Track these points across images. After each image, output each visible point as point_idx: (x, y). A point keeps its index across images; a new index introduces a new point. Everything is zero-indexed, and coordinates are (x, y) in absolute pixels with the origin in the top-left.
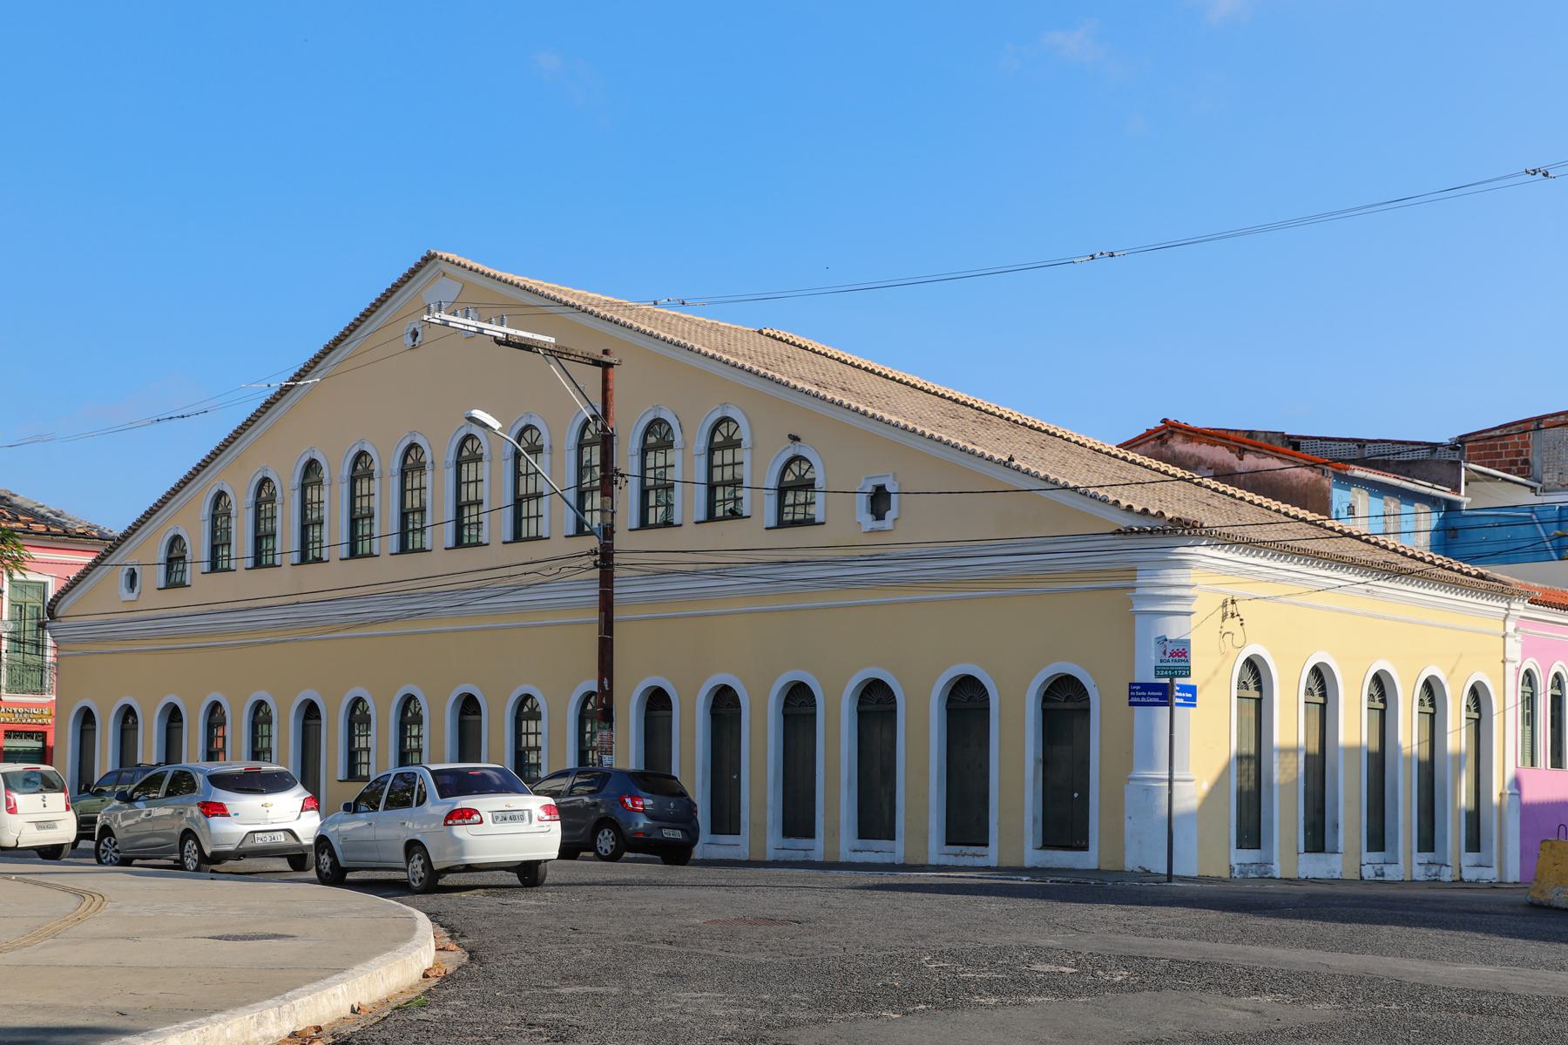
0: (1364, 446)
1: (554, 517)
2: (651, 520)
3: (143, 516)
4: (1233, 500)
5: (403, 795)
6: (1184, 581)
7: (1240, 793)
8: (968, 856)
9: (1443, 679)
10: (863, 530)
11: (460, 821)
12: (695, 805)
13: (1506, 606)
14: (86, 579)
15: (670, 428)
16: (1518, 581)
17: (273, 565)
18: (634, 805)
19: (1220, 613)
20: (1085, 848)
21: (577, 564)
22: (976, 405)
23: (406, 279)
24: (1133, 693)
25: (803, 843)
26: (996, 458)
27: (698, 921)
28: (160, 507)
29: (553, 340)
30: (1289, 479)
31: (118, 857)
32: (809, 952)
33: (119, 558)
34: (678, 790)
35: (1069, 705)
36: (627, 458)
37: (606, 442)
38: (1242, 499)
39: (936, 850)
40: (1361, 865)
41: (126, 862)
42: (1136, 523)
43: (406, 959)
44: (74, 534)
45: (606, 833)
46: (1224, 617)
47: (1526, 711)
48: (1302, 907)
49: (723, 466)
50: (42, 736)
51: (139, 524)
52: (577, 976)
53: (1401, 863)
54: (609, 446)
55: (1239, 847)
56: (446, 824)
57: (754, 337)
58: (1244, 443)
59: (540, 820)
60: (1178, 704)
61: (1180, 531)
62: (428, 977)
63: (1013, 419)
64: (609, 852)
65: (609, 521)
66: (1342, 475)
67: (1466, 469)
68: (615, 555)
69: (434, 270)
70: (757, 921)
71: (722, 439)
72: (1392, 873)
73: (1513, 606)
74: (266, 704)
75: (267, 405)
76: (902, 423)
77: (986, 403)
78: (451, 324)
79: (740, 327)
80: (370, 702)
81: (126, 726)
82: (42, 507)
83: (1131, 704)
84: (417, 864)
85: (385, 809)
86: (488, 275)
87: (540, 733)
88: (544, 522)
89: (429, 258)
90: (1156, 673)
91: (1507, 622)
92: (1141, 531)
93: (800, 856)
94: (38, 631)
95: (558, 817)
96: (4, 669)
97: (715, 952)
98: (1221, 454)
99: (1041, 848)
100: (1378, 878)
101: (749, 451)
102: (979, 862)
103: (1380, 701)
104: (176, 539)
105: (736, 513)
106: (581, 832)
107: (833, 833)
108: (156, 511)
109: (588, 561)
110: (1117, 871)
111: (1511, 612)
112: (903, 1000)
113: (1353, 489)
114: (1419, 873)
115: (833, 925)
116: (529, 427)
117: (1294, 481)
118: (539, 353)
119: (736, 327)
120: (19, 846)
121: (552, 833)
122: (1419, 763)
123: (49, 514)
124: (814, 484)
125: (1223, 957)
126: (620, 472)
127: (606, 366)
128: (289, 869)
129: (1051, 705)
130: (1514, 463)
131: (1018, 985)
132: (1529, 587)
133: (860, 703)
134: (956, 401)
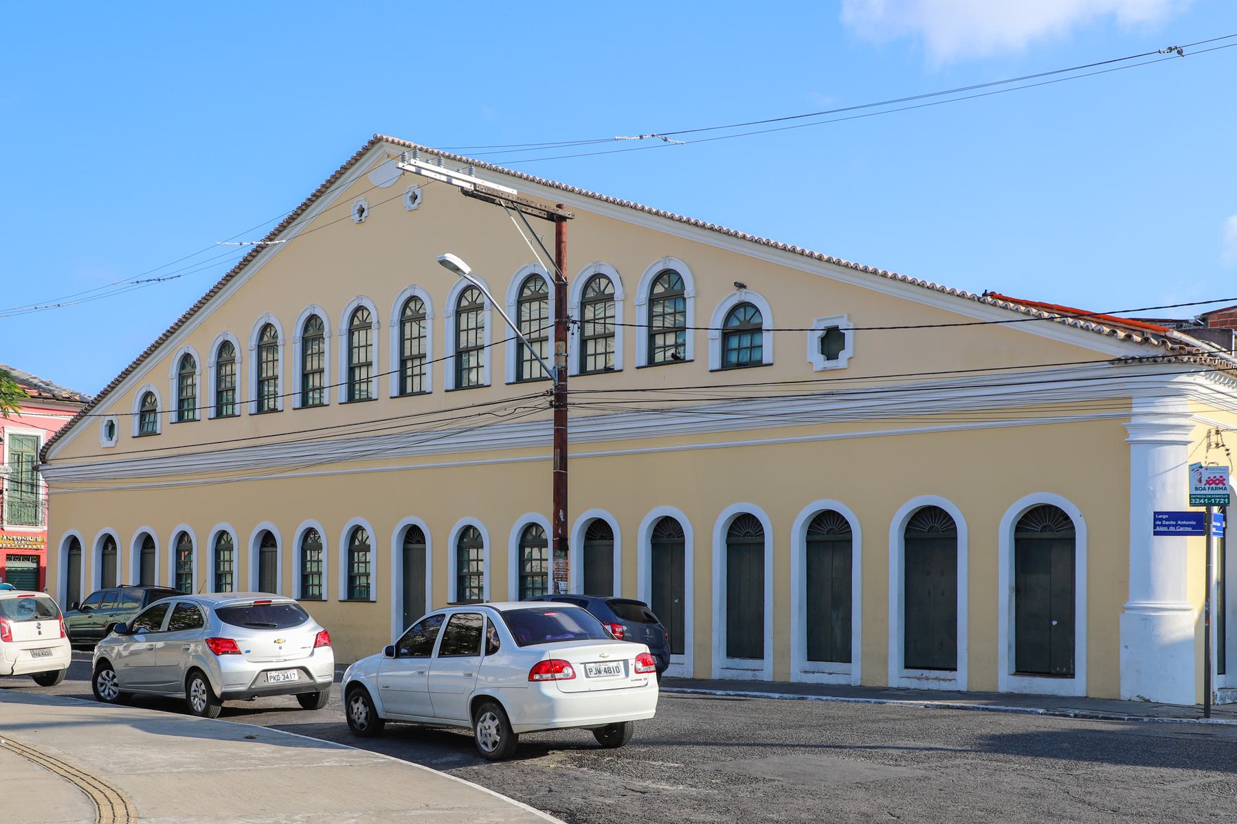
3: (120, 376)
6: (1181, 410)
10: (815, 369)
11: (549, 676)
14: (72, 430)
21: (533, 404)
23: (353, 161)
29: (515, 192)
31: (117, 692)
33: (103, 408)
44: (60, 398)
46: (1209, 446)
50: (37, 559)
51: (117, 382)
54: (563, 295)
65: (564, 364)
68: (568, 395)
69: (380, 152)
74: (228, 533)
75: (227, 278)
78: (423, 172)
80: (233, 534)
81: (107, 552)
82: (35, 378)
83: (1156, 533)
85: (441, 655)
87: (482, 560)
90: (1190, 501)
93: (748, 676)
94: (32, 472)
96: (5, 505)
99: (1014, 675)
102: (945, 686)
107: (783, 655)
109: (545, 401)
118: (501, 205)
120: (14, 674)
123: (40, 384)
128: (299, 706)
133: (809, 533)
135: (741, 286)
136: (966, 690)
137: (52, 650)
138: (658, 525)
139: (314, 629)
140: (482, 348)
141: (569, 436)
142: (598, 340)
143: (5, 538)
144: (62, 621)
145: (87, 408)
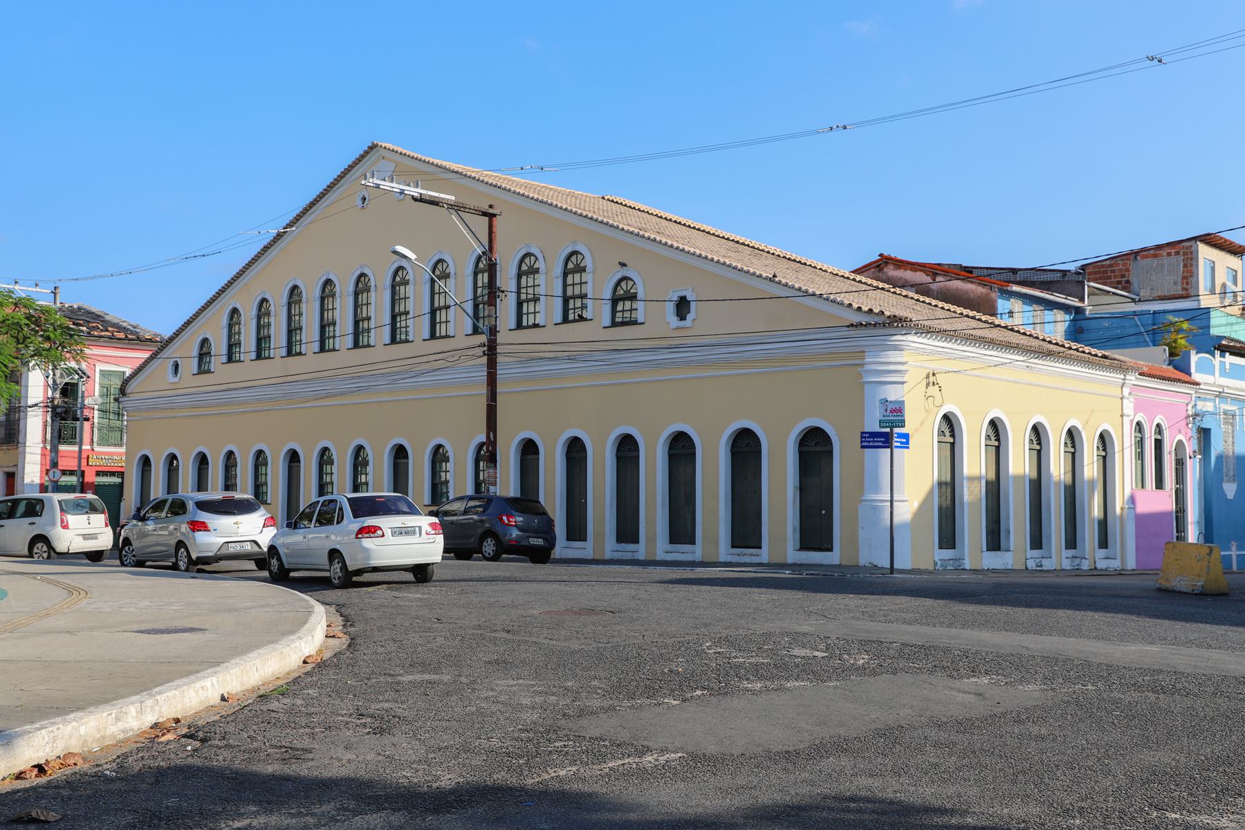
0: (1017, 273)
1: (458, 322)
2: (525, 323)
3: (183, 326)
4: (930, 307)
5: (327, 516)
6: (899, 360)
7: (940, 508)
8: (747, 555)
9: (1080, 427)
11: (368, 535)
12: (553, 521)
13: (1123, 377)
15: (537, 259)
16: (1130, 360)
17: (269, 358)
18: (509, 521)
19: (924, 382)
20: (831, 550)
22: (751, 245)
23: (357, 162)
24: (863, 439)
25: (631, 547)
26: (764, 276)
27: (535, 612)
28: (194, 319)
29: (453, 198)
30: (967, 293)
32: (615, 640)
33: (169, 352)
34: (541, 511)
35: (818, 449)
36: (506, 279)
37: (492, 269)
38: (936, 306)
39: (724, 551)
41: (140, 564)
42: (864, 319)
43: (284, 650)
44: (144, 339)
45: (489, 541)
46: (928, 385)
47: (1138, 450)
48: (994, 594)
49: (573, 285)
52: (423, 664)
53: (1054, 557)
55: (941, 548)
56: (357, 538)
57: (598, 201)
58: (936, 269)
59: (427, 534)
60: (896, 447)
61: (896, 324)
62: (307, 663)
63: (777, 254)
64: (492, 554)
65: (494, 323)
66: (1004, 290)
67: (1088, 286)
68: (498, 347)
70: (581, 612)
71: (573, 266)
72: (1048, 564)
73: (1128, 377)
74: (443, 447)
76: (698, 252)
77: (758, 244)
78: (381, 187)
79: (589, 194)
80: (333, 451)
81: (172, 468)
82: (125, 322)
83: (863, 447)
84: (337, 566)
86: (413, 157)
88: (451, 326)
89: (373, 147)
91: (1124, 389)
92: (868, 325)
93: (629, 556)
95: (441, 532)
97: (541, 640)
98: (921, 277)
99: (799, 550)
100: (1038, 568)
101: (592, 274)
103: (1037, 444)
104: (205, 341)
105: (583, 317)
106: (472, 540)
107: (652, 539)
108: (191, 322)
109: (479, 351)
110: (853, 566)
111: (1127, 381)
112: (682, 685)
113: (1012, 300)
114: (1067, 565)
115: (637, 615)
116: (441, 261)
117: (971, 294)
119: (594, 196)
120: (70, 552)
121: (437, 543)
122: (1065, 487)
123: (129, 327)
124: (636, 297)
125: (943, 641)
126: (502, 289)
127: (491, 216)
128: (256, 568)
129: (804, 449)
130: (1119, 282)
131: (780, 669)
132: (1137, 364)
133: (670, 448)
134: (737, 242)
135: (623, 265)
136: (767, 562)
137: (98, 536)
138: (570, 443)
139: (262, 516)
140: (449, 307)
141: (498, 377)
142: (529, 303)
143: (95, 457)
144: (107, 515)
145: (161, 346)
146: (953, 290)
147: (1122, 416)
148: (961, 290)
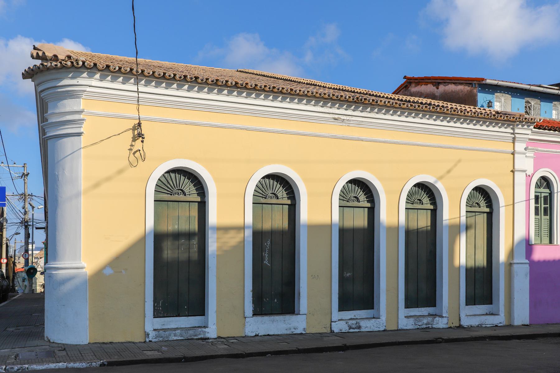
6: (76, 109)
13: (512, 131)
40: (332, 322)
73: (517, 131)
98: (430, 88)
111: (517, 136)
117: (461, 94)
146: (449, 93)
147: (513, 171)
148: (454, 92)
